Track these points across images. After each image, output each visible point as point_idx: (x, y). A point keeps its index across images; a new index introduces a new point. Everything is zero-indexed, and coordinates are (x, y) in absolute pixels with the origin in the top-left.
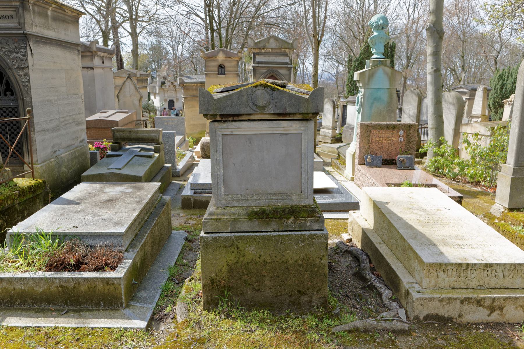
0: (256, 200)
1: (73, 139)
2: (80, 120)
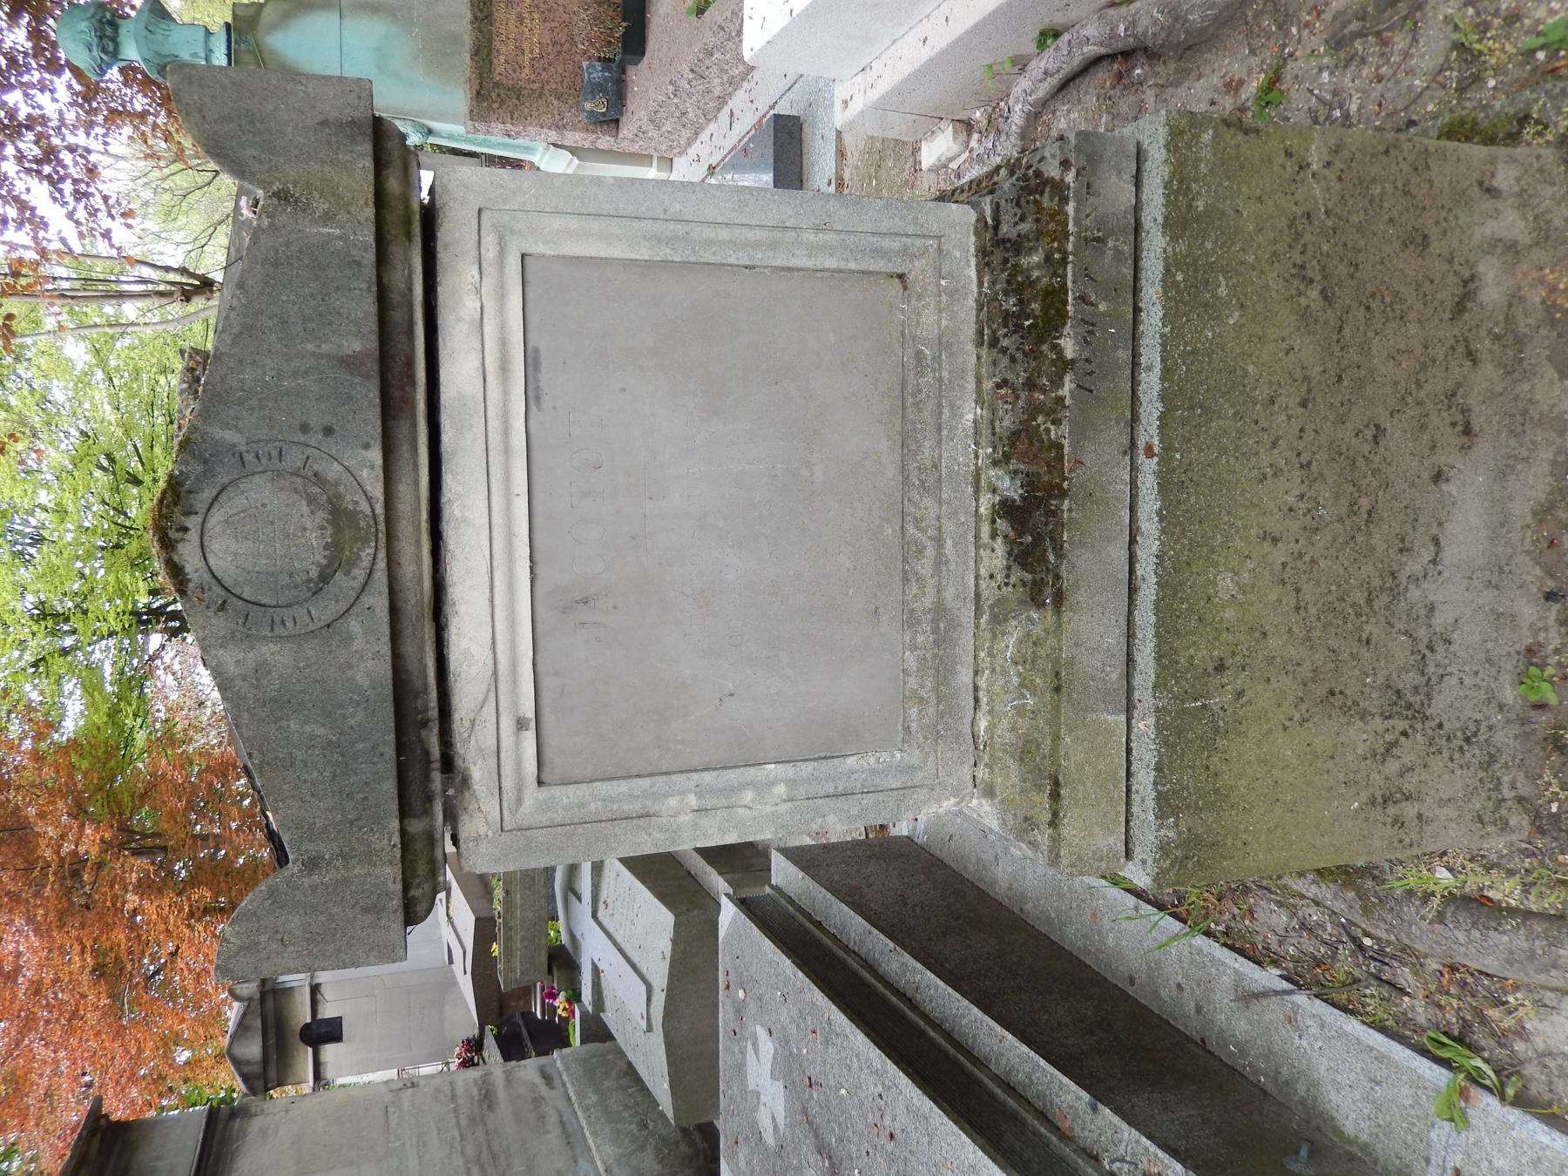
0: (940, 561)
1: (542, 1118)
2: (475, 1092)
